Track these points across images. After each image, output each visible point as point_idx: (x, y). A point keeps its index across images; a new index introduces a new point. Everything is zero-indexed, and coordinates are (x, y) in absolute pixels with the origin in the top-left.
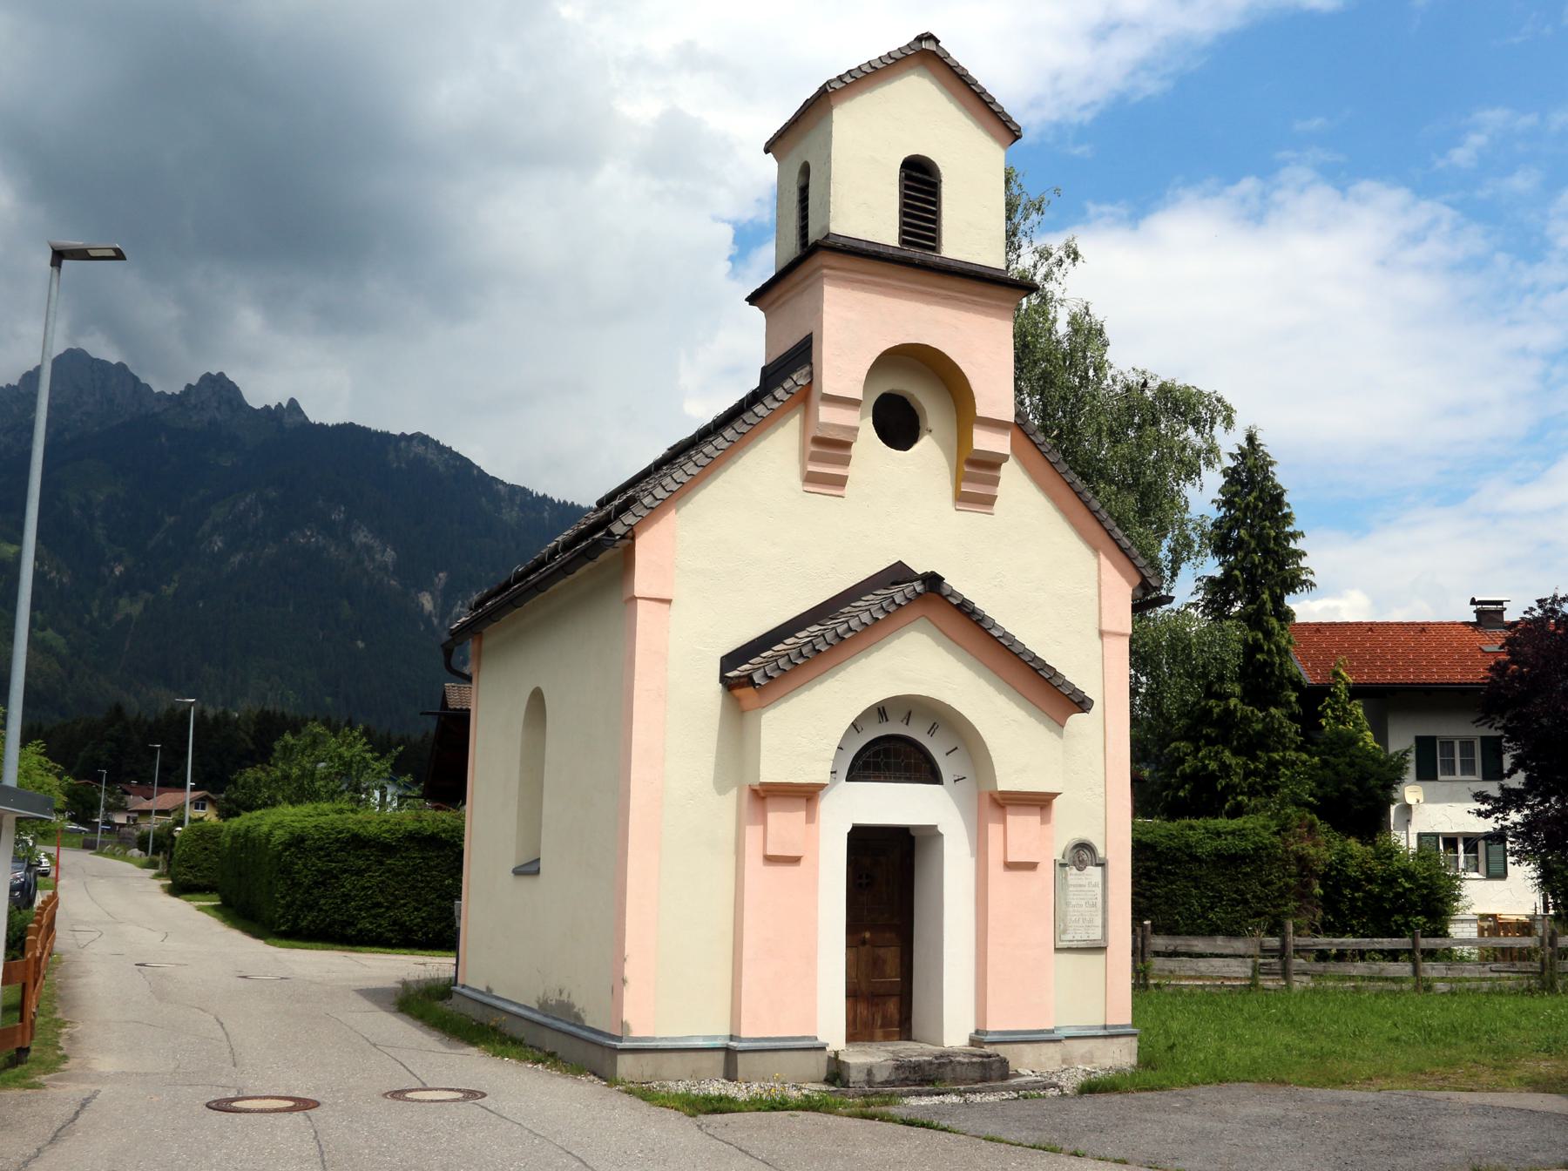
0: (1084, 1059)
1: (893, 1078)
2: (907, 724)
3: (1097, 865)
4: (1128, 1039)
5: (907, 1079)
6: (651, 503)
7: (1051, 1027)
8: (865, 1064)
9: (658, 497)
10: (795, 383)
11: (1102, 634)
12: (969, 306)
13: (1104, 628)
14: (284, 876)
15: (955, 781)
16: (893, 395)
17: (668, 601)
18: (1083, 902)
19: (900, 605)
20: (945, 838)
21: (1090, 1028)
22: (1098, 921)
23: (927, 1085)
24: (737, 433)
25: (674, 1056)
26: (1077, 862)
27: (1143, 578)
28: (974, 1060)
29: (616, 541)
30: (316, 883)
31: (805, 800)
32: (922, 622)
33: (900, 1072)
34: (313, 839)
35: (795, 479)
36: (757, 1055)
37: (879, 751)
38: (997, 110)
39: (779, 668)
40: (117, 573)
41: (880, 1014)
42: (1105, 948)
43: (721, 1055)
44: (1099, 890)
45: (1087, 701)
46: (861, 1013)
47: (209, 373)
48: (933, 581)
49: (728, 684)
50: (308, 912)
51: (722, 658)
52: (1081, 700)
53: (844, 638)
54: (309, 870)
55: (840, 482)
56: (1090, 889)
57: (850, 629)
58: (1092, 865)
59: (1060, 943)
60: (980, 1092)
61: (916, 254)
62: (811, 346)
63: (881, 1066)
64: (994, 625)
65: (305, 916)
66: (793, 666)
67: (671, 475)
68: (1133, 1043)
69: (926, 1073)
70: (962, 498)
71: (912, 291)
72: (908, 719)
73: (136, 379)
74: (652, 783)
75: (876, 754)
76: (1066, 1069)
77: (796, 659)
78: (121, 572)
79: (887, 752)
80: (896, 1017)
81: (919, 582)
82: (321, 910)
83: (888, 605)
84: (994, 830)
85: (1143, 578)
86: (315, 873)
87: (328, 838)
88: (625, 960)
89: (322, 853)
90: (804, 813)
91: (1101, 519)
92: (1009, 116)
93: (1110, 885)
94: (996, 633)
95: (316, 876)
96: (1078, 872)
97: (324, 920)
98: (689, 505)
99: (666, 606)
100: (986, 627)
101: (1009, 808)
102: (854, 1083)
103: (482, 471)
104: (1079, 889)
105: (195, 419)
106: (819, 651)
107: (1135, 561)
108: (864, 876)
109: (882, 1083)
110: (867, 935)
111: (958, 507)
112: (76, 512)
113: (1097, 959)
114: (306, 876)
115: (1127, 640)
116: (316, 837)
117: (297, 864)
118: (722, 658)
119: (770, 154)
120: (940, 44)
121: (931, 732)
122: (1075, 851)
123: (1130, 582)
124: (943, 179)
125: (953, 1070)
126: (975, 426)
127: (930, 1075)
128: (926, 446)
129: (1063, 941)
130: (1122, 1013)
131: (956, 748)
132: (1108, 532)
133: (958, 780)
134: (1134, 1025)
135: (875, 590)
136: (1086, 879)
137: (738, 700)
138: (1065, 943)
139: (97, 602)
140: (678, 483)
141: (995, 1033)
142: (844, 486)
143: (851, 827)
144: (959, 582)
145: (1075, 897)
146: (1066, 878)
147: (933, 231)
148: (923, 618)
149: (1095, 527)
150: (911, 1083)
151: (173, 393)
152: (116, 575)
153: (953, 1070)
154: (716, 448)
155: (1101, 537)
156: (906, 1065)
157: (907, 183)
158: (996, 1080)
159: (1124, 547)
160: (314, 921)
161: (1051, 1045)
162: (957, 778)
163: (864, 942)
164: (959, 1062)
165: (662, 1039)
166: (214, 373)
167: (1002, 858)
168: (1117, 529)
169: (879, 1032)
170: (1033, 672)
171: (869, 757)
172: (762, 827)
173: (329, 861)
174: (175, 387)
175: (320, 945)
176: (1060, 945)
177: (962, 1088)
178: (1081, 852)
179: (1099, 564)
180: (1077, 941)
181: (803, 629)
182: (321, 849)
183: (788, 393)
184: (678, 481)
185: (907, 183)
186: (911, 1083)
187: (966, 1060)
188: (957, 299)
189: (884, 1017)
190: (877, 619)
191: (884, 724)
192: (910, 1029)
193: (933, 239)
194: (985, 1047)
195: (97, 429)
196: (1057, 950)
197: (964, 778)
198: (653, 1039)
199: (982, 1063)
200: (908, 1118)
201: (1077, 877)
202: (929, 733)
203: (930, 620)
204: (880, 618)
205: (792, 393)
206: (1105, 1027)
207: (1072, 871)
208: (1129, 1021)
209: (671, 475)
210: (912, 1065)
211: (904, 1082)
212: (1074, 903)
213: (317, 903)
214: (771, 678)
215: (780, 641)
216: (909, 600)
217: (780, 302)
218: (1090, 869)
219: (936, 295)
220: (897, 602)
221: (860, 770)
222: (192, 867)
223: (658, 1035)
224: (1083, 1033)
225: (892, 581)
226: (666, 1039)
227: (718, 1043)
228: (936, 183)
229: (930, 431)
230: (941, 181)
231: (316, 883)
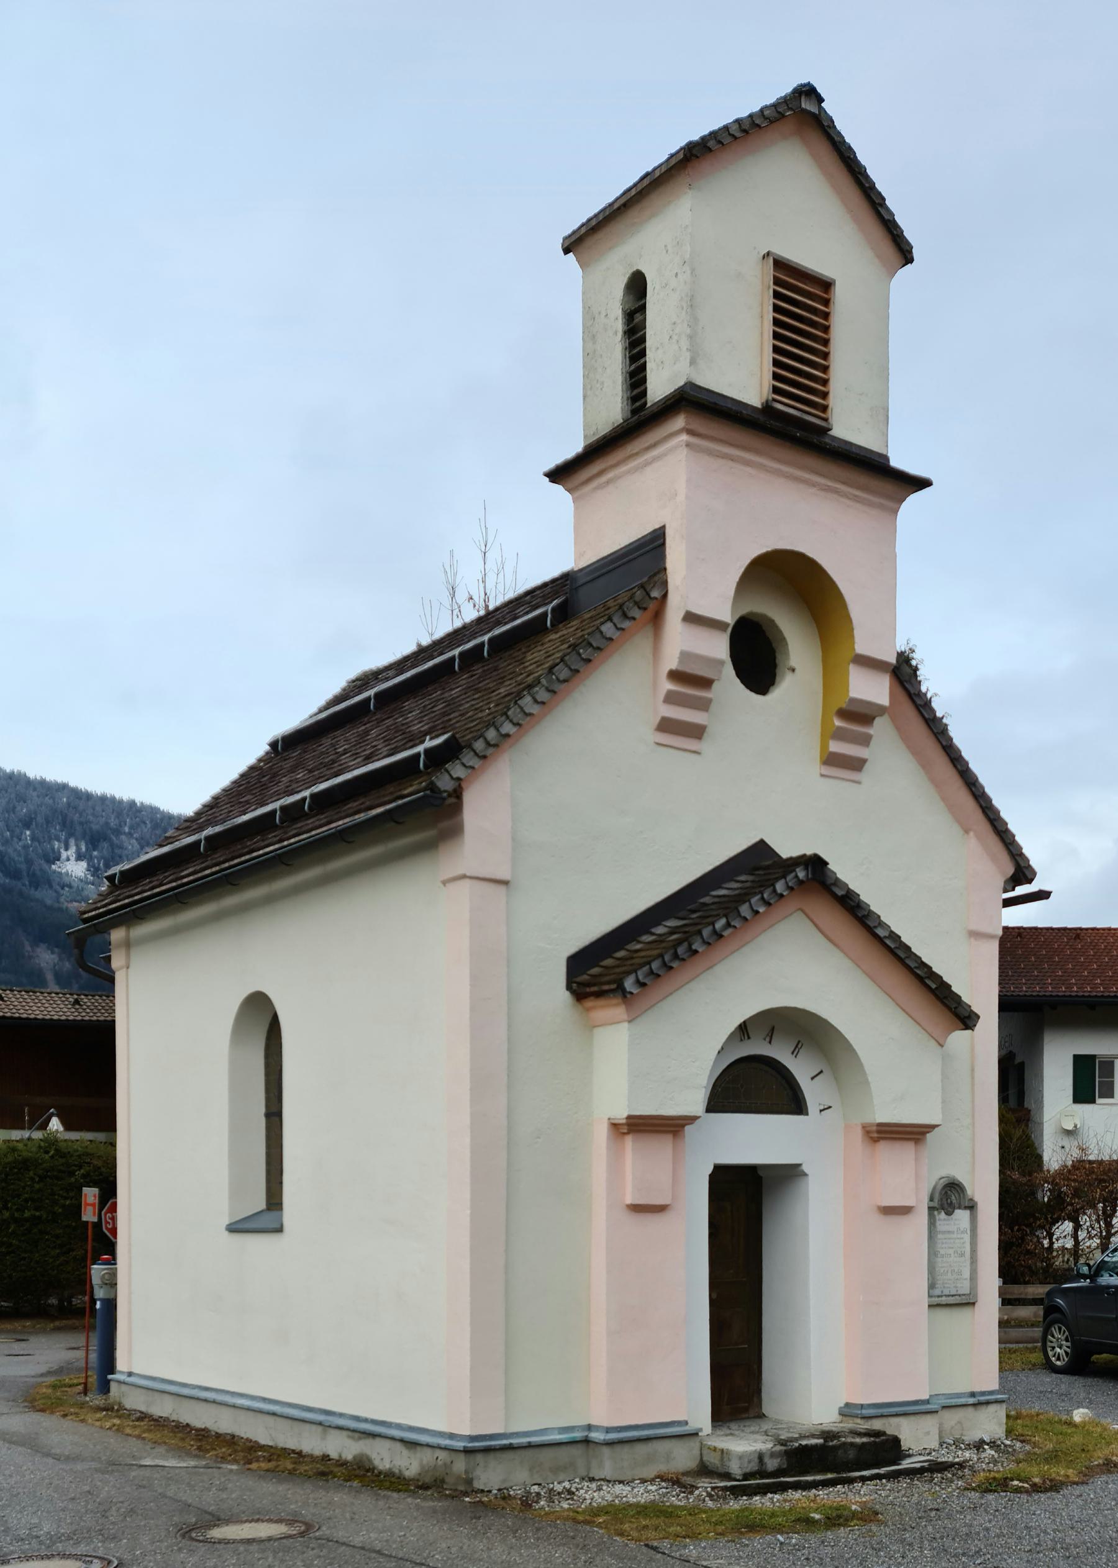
2: (770, 1042)
3: (966, 1208)
15: (821, 1111)
22: (966, 1274)
26: (946, 1206)
29: (444, 799)
38: (887, 217)
44: (967, 1238)
45: (973, 1016)
48: (816, 864)
56: (959, 1236)
58: (959, 1208)
62: (664, 544)
64: (881, 924)
77: (671, 961)
81: (802, 867)
94: (881, 932)
103: (857, 158)
107: (1011, 847)
120: (823, 105)
121: (795, 1052)
130: (988, 1378)
134: (1003, 1388)
135: (737, 876)
136: (955, 1224)
143: (712, 1167)
144: (843, 869)
161: (929, 1417)
162: (822, 1108)
180: (946, 1296)
181: (658, 924)
188: (836, 491)
191: (747, 1042)
197: (830, 1107)
202: (793, 1053)
208: (995, 1386)
215: (634, 939)
219: (813, 485)
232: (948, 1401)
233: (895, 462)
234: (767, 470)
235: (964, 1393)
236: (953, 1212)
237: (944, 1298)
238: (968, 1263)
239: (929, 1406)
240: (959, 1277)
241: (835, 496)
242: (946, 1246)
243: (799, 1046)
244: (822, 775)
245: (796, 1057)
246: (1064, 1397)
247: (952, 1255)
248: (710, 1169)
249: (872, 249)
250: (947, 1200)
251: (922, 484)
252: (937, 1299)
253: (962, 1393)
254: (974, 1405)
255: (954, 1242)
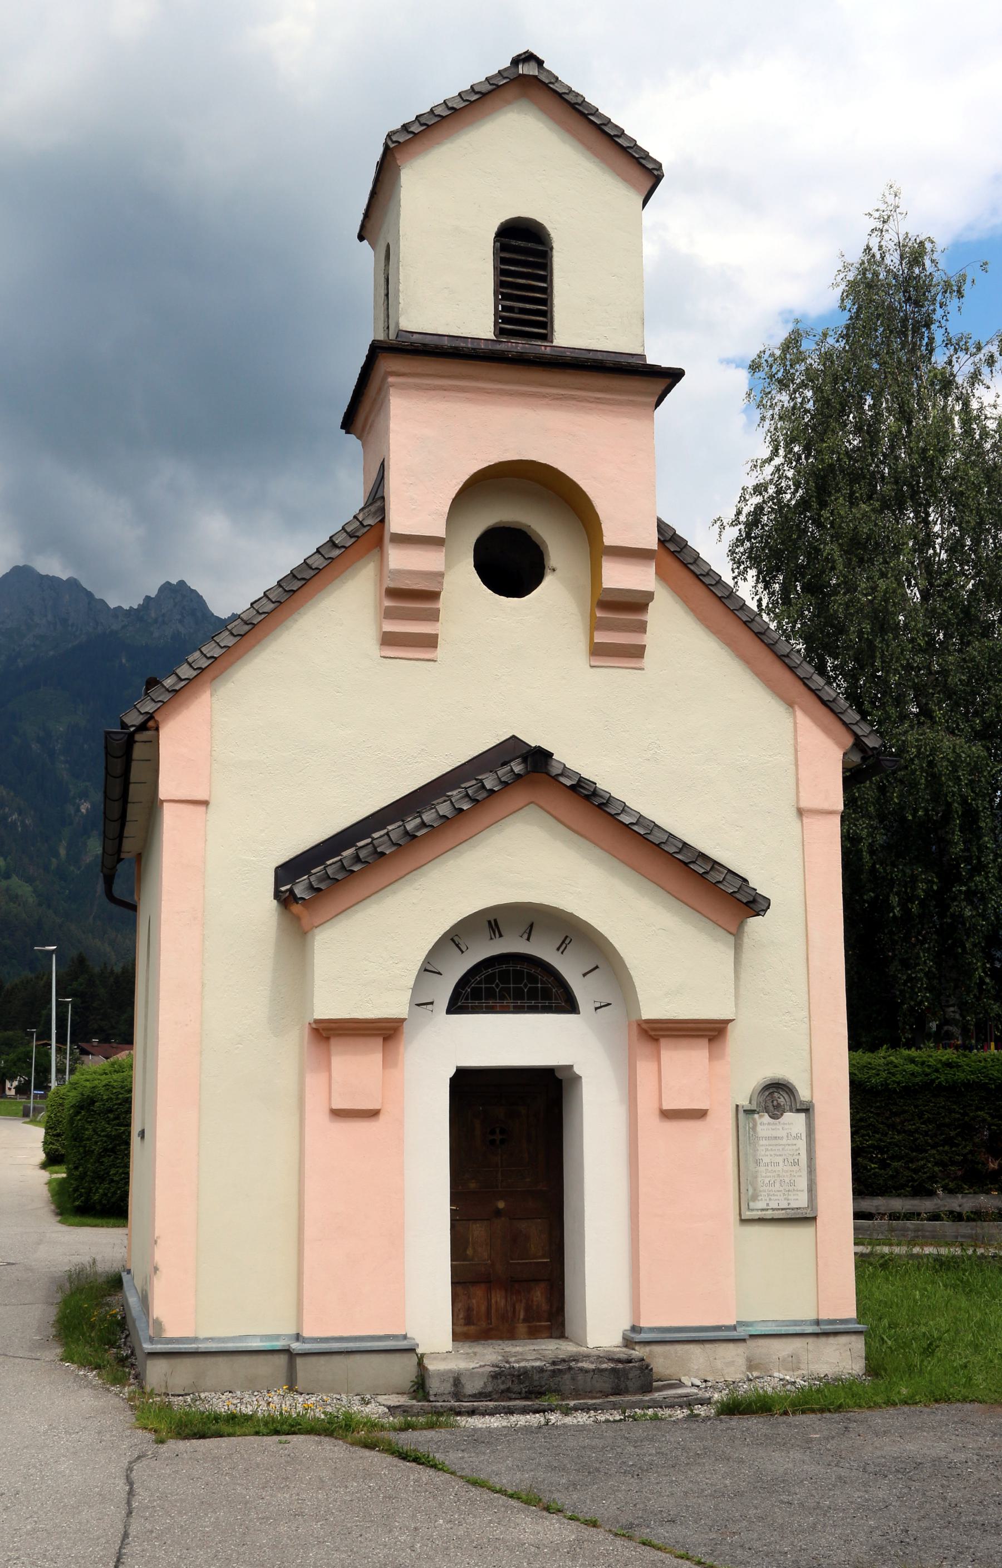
0: (785, 1363)
1: (490, 1389)
2: (528, 939)
3: (798, 1111)
4: (853, 1338)
5: (508, 1390)
6: (174, 685)
7: (731, 1322)
8: (450, 1371)
9: (183, 677)
10: (361, 523)
11: (800, 812)
12: (593, 405)
13: (804, 804)
14: (78, 1144)
15: (596, 1009)
16: (504, 527)
17: (205, 803)
18: (780, 1159)
19: (492, 792)
20: (585, 1082)
21: (796, 1323)
22: (803, 1183)
23: (536, 1398)
24: (285, 591)
25: (221, 1360)
26: (771, 1108)
27: (857, 738)
28: (604, 1366)
30: (106, 1150)
31: (380, 1040)
32: (532, 811)
33: (499, 1381)
34: (102, 1100)
35: (370, 643)
36: (322, 1360)
37: (494, 974)
39: (329, 877)
40: (83, 811)
41: (523, 1305)
42: (815, 1218)
43: (282, 1360)
44: (802, 1145)
45: (759, 900)
46: (496, 1302)
47: (168, 583)
49: (285, 899)
50: (100, 1184)
51: (277, 869)
52: (751, 899)
53: (416, 836)
54: (100, 1136)
55: (430, 642)
56: (789, 1142)
57: (423, 825)
58: (791, 1111)
59: (748, 1213)
60: (595, 1410)
61: (517, 346)
63: (472, 1374)
64: (625, 808)
65: (97, 1188)
66: (349, 873)
67: (200, 649)
68: (858, 1344)
69: (536, 1383)
70: (598, 651)
71: (511, 394)
72: (529, 933)
73: (89, 595)
74: (187, 1025)
75: (490, 979)
76: (758, 1378)
77: (351, 866)
78: (87, 810)
79: (504, 976)
80: (545, 1307)
81: (519, 760)
82: (112, 1181)
83: (476, 792)
84: (645, 1069)
85: (857, 738)
86: (105, 1139)
87: (117, 1099)
88: (156, 1242)
89: (111, 1116)
90: (381, 1055)
91: (792, 664)
92: (658, 162)
93: (819, 1136)
94: (626, 819)
95: (106, 1142)
96: (772, 1121)
97: (115, 1193)
98: (230, 685)
99: (202, 809)
100: (613, 812)
101: (663, 1042)
102: (435, 1395)
104: (774, 1142)
105: (156, 634)
106: (382, 854)
108: (498, 1131)
109: (474, 1396)
110: (501, 1205)
111: (593, 664)
112: (35, 747)
113: (801, 1233)
114: (96, 1143)
115: (837, 820)
116: (105, 1097)
117: (87, 1129)
118: (277, 868)
119: (365, 241)
122: (767, 1093)
123: (839, 744)
124: (555, 245)
125: (573, 1379)
126: (604, 558)
127: (541, 1387)
128: (549, 589)
129: (753, 1210)
131: (597, 967)
132: (804, 681)
133: (601, 1007)
135: (480, 774)
137: (297, 919)
138: (755, 1213)
139: (64, 843)
140: (208, 658)
141: (652, 1330)
142: (436, 647)
143: (454, 1070)
145: (768, 1153)
146: (754, 1128)
147: (544, 314)
148: (532, 805)
149: (786, 676)
150: (514, 1396)
151: (131, 607)
152: (82, 813)
153: (573, 1379)
154: (258, 612)
155: (797, 689)
156: (506, 1372)
157: (503, 255)
158: (635, 1393)
159: (826, 698)
160: (105, 1195)
161: (731, 1346)
162: (598, 1005)
163: (498, 1213)
164: (581, 1369)
165: (207, 1339)
166: (174, 581)
167: (656, 1106)
168: (816, 677)
169: (522, 1328)
170: (684, 866)
171: (480, 982)
172: (656, 1063)
173: (118, 1125)
174: (132, 601)
175: (112, 1221)
176: (747, 1215)
177: (572, 1403)
178: (776, 1094)
179: (795, 723)
180: (773, 1209)
182: (111, 1111)
183: (351, 537)
184: (208, 655)
185: (503, 255)
186: (514, 1396)
187: (592, 1366)
188: (573, 398)
189: (528, 1309)
190: (461, 810)
192: (563, 1324)
193: (544, 325)
194: (637, 1348)
195: (51, 653)
196: (744, 1221)
197: (609, 1004)
198: (195, 1340)
199: (613, 1370)
200: (405, 1448)
201: (770, 1127)
202: (558, 949)
203: (541, 807)
204: (465, 808)
205: (358, 537)
206: (817, 1322)
207: (764, 1120)
208: (853, 1314)
209: (200, 649)
210: (516, 1373)
211: (505, 1394)
212: (766, 1160)
213: (108, 1173)
214: (319, 890)
216: (506, 784)
217: (368, 427)
218: (789, 1116)
220: (488, 787)
221: (467, 999)
222: (58, 1135)
223: (202, 1335)
224: (784, 1330)
225: (500, 763)
226: (212, 1339)
227: (278, 1344)
228: (546, 252)
229: (554, 570)
230: (552, 249)
231: (106, 1150)
232: (779, 1328)
233: (653, 359)
234: (488, 393)
235: (806, 1321)
236: (782, 1115)
237: (770, 1212)
238: (804, 1173)
239: (734, 1333)
240: (791, 1188)
241: (574, 402)
242: (772, 1153)
243: (567, 942)
244: (592, 667)
245: (562, 953)
246: (952, 1333)
247: (781, 1164)
248: (452, 1072)
249: (618, 175)
250: (773, 1102)
251: (673, 376)
252: (759, 1213)
253: (802, 1321)
254: (816, 1335)
255: (783, 1149)
